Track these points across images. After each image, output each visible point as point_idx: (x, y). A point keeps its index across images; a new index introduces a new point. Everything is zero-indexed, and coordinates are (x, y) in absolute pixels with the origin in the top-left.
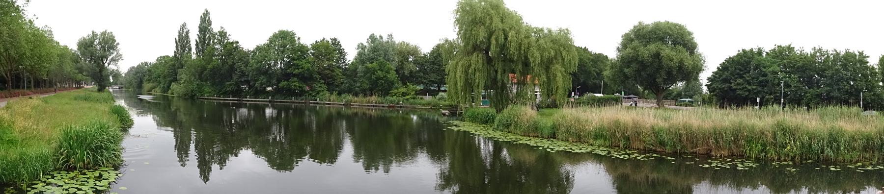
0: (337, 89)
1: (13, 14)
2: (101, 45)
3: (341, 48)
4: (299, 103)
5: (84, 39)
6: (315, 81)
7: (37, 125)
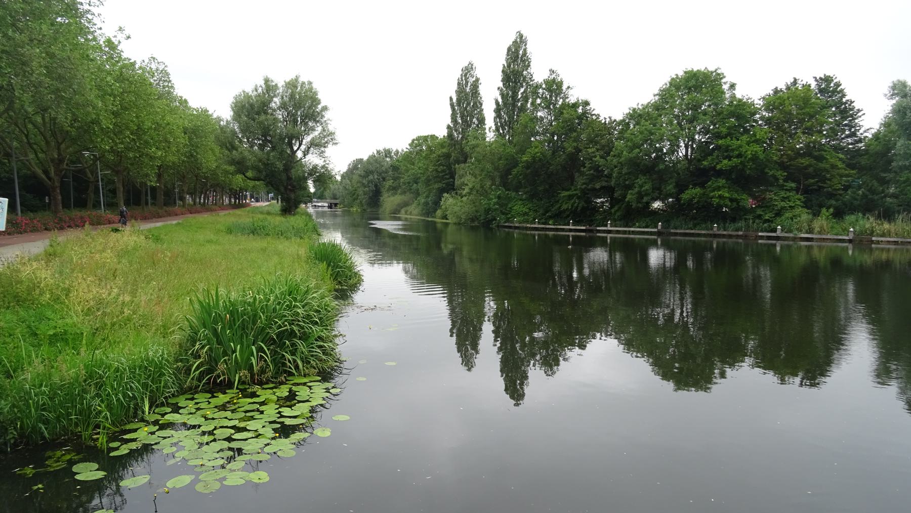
0: (833, 202)
1: (59, 19)
2: (286, 109)
3: (844, 100)
4: (730, 236)
5: (247, 96)
6: (772, 185)
7: (133, 293)
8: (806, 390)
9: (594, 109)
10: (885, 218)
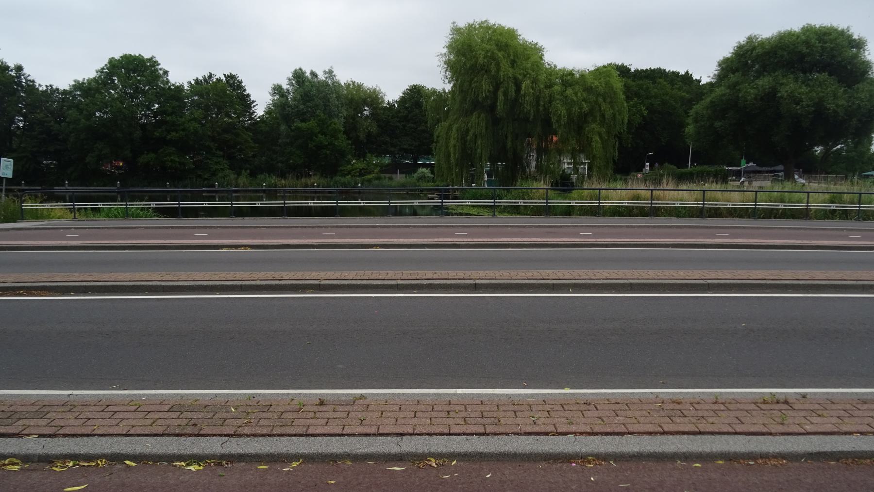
8: (780, 30)
9: (29, 75)
10: (282, 177)
